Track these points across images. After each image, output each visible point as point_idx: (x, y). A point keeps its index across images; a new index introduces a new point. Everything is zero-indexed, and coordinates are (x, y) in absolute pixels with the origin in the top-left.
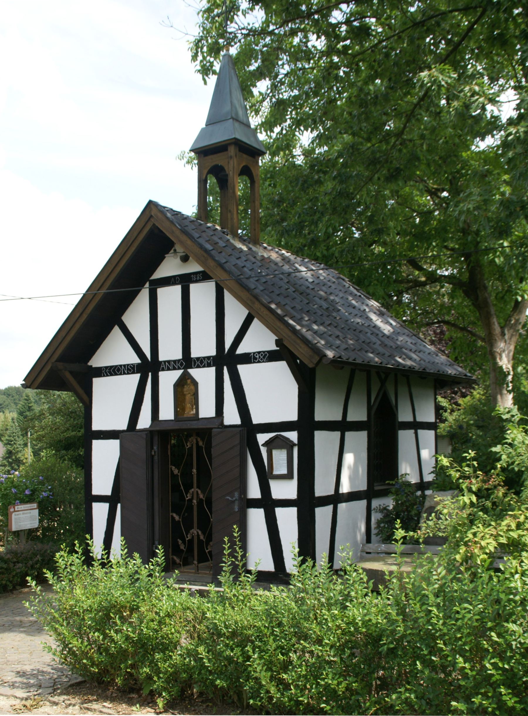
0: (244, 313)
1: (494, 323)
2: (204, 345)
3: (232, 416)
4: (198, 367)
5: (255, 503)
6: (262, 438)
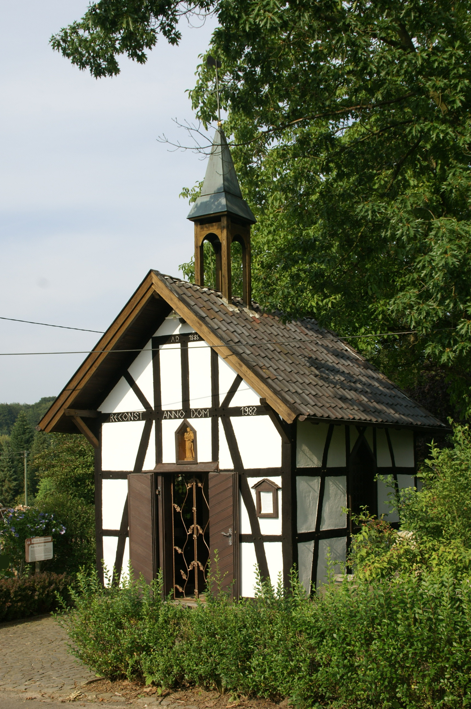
2: (201, 398)
4: (196, 417)
5: (247, 538)
6: (252, 481)
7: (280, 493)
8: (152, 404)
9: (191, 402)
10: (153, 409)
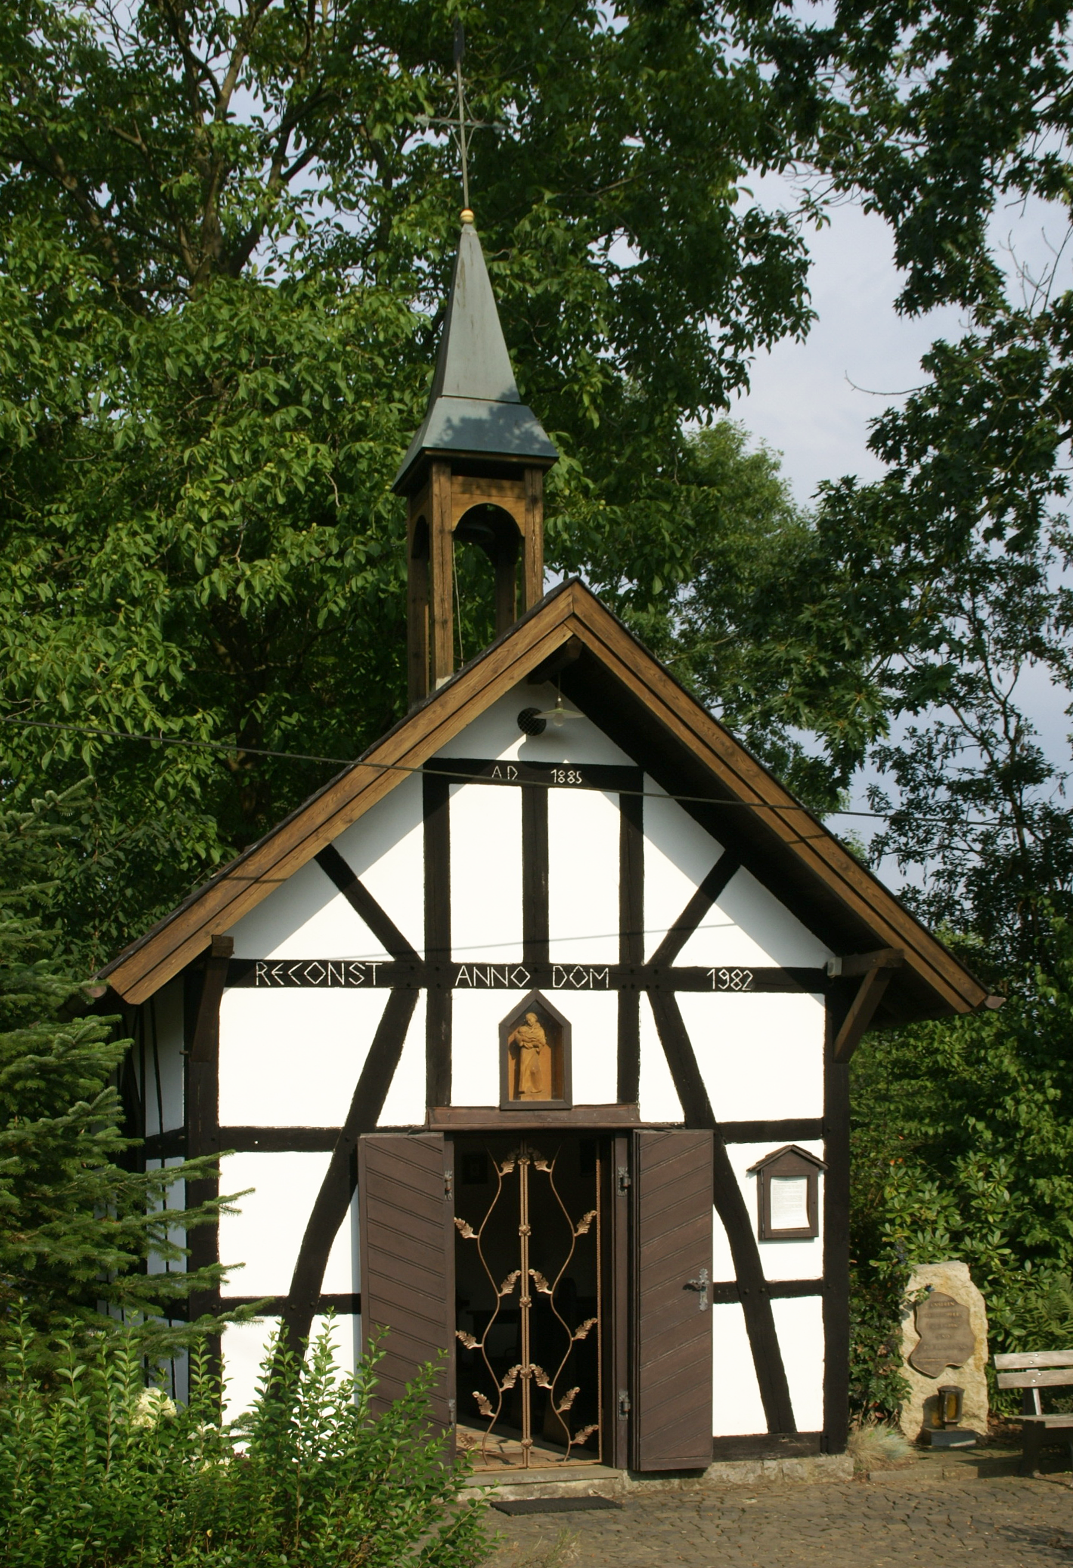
0: (689, 889)
2: (586, 931)
3: (659, 1102)
4: (568, 986)
5: (724, 1293)
6: (742, 1157)
7: (821, 1179)
8: (417, 940)
9: (553, 947)
10: (422, 956)
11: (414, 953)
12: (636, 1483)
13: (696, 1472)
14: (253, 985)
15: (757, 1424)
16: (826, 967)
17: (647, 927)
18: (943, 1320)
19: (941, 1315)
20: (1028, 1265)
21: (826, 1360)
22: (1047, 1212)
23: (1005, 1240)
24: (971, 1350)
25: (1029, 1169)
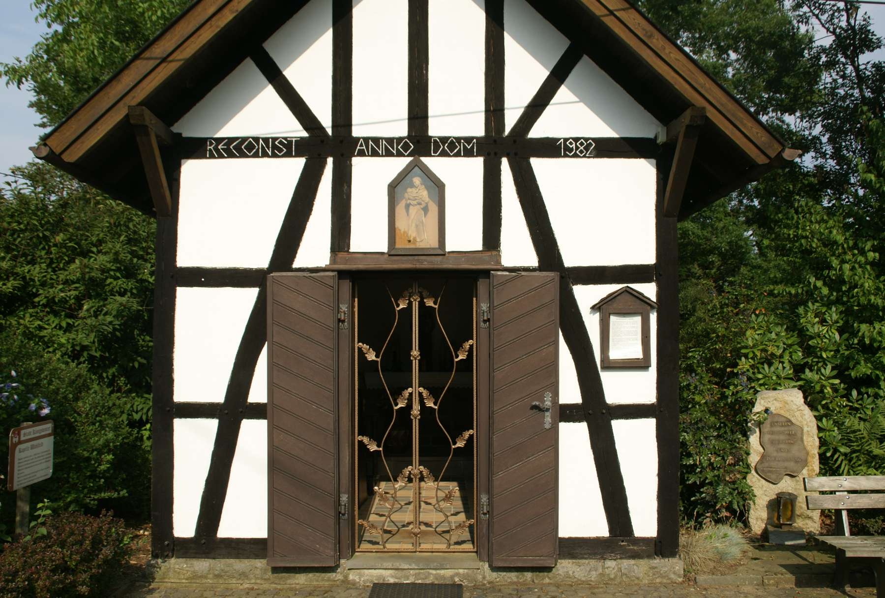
0: (541, 74)
1: (437, 577)
2: (457, 109)
4: (444, 154)
5: (569, 413)
6: (587, 296)
7: (653, 317)
9: (431, 122)
10: (329, 131)
11: (322, 129)
12: (495, 574)
13: (549, 569)
14: (204, 157)
15: (597, 526)
16: (656, 137)
17: (507, 104)
18: (782, 437)
19: (780, 433)
20: (854, 393)
21: (659, 475)
22: (869, 350)
23: (835, 372)
24: (805, 463)
25: (856, 313)
